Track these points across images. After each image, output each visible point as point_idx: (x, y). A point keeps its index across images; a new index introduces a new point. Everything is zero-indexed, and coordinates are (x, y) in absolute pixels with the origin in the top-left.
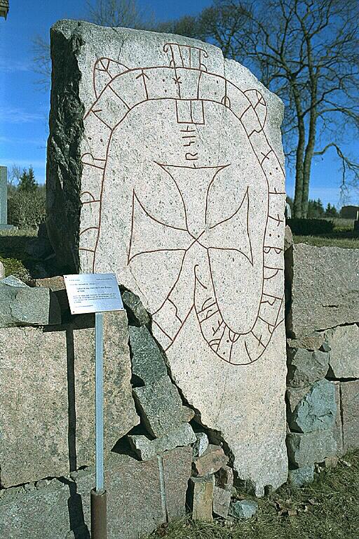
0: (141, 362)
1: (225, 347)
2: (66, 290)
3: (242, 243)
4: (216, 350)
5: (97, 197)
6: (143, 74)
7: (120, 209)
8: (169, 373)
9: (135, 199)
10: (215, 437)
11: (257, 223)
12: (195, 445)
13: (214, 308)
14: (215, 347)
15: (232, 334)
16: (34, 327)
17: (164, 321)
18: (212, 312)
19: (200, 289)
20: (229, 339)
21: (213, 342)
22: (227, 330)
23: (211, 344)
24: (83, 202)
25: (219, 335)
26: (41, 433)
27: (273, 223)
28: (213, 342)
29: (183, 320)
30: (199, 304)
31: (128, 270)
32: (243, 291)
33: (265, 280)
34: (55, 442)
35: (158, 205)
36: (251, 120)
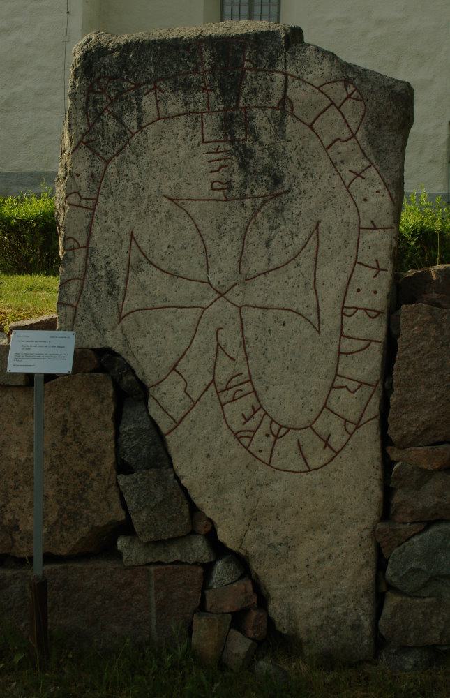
0: (129, 443)
1: (261, 442)
2: (8, 347)
3: (304, 302)
4: (246, 445)
5: (82, 242)
6: (154, 88)
7: (112, 257)
8: (171, 465)
9: (134, 244)
10: (242, 563)
11: (331, 275)
12: (208, 568)
13: (247, 387)
14: (246, 441)
15: (275, 427)
16: (8, 386)
17: (168, 399)
18: (244, 392)
19: (224, 360)
20: (269, 432)
21: (242, 434)
22: (267, 419)
23: (239, 435)
24: (230, 616)
25: (252, 424)
26: (282, 150)
27: (366, 275)
28: (242, 434)
29: (195, 397)
30: (222, 377)
31: (118, 330)
32: (300, 368)
33: (343, 356)
34: (16, 517)
35: (165, 250)
36: (331, 125)
